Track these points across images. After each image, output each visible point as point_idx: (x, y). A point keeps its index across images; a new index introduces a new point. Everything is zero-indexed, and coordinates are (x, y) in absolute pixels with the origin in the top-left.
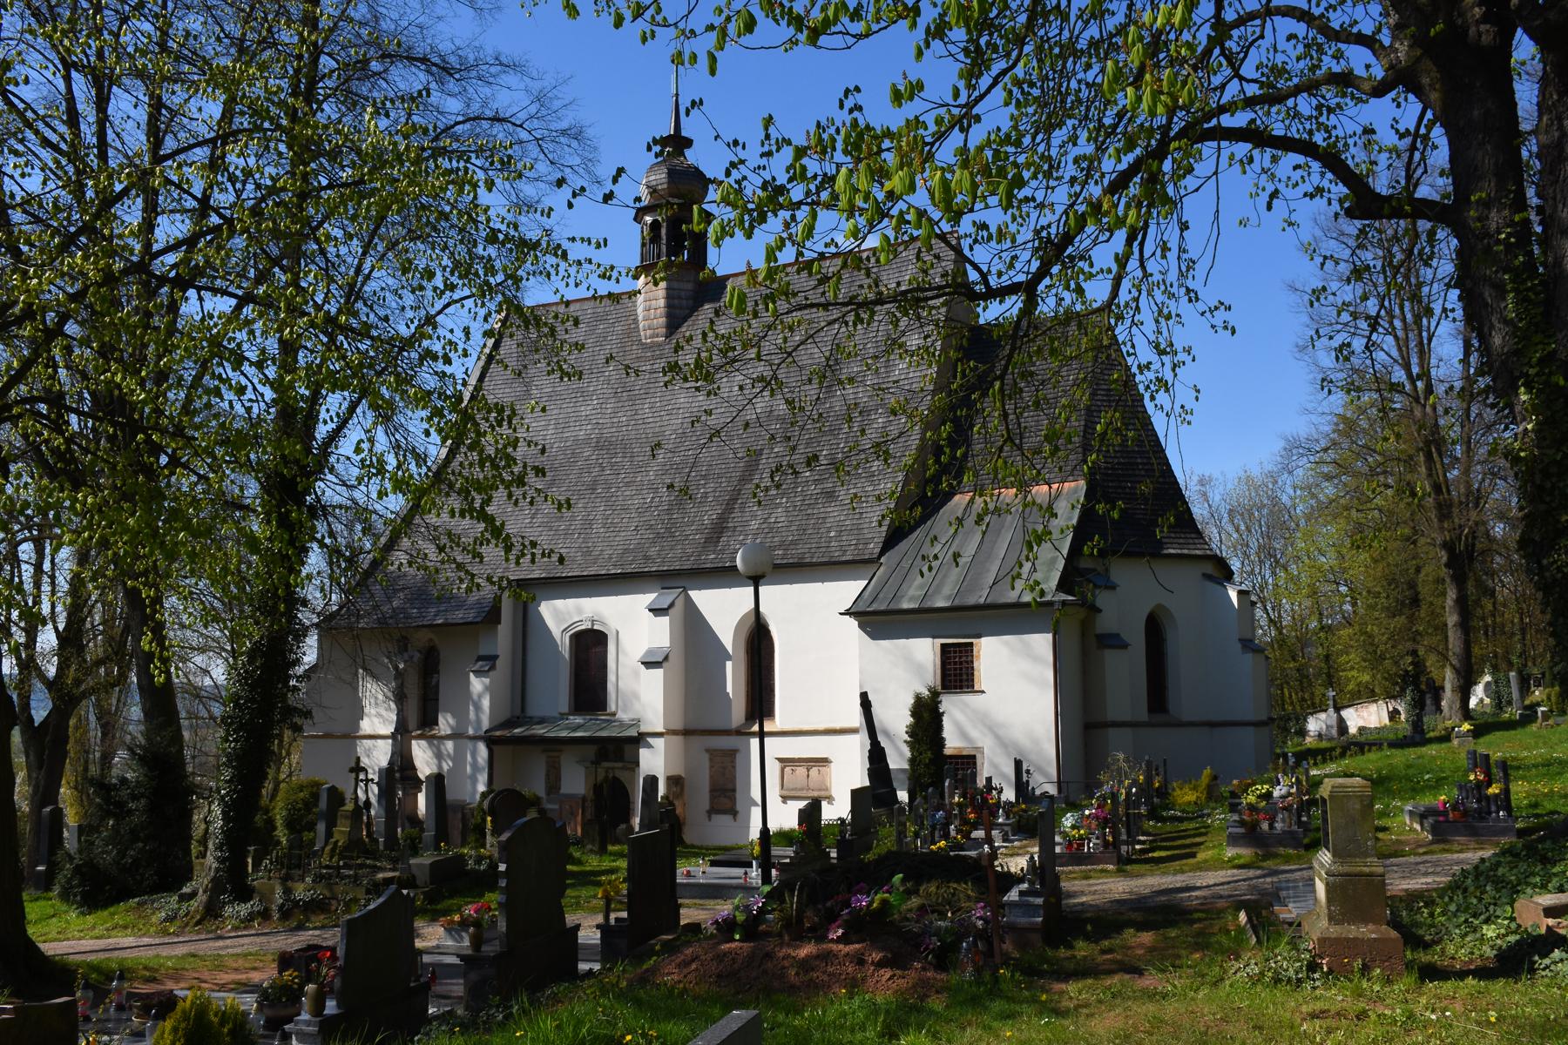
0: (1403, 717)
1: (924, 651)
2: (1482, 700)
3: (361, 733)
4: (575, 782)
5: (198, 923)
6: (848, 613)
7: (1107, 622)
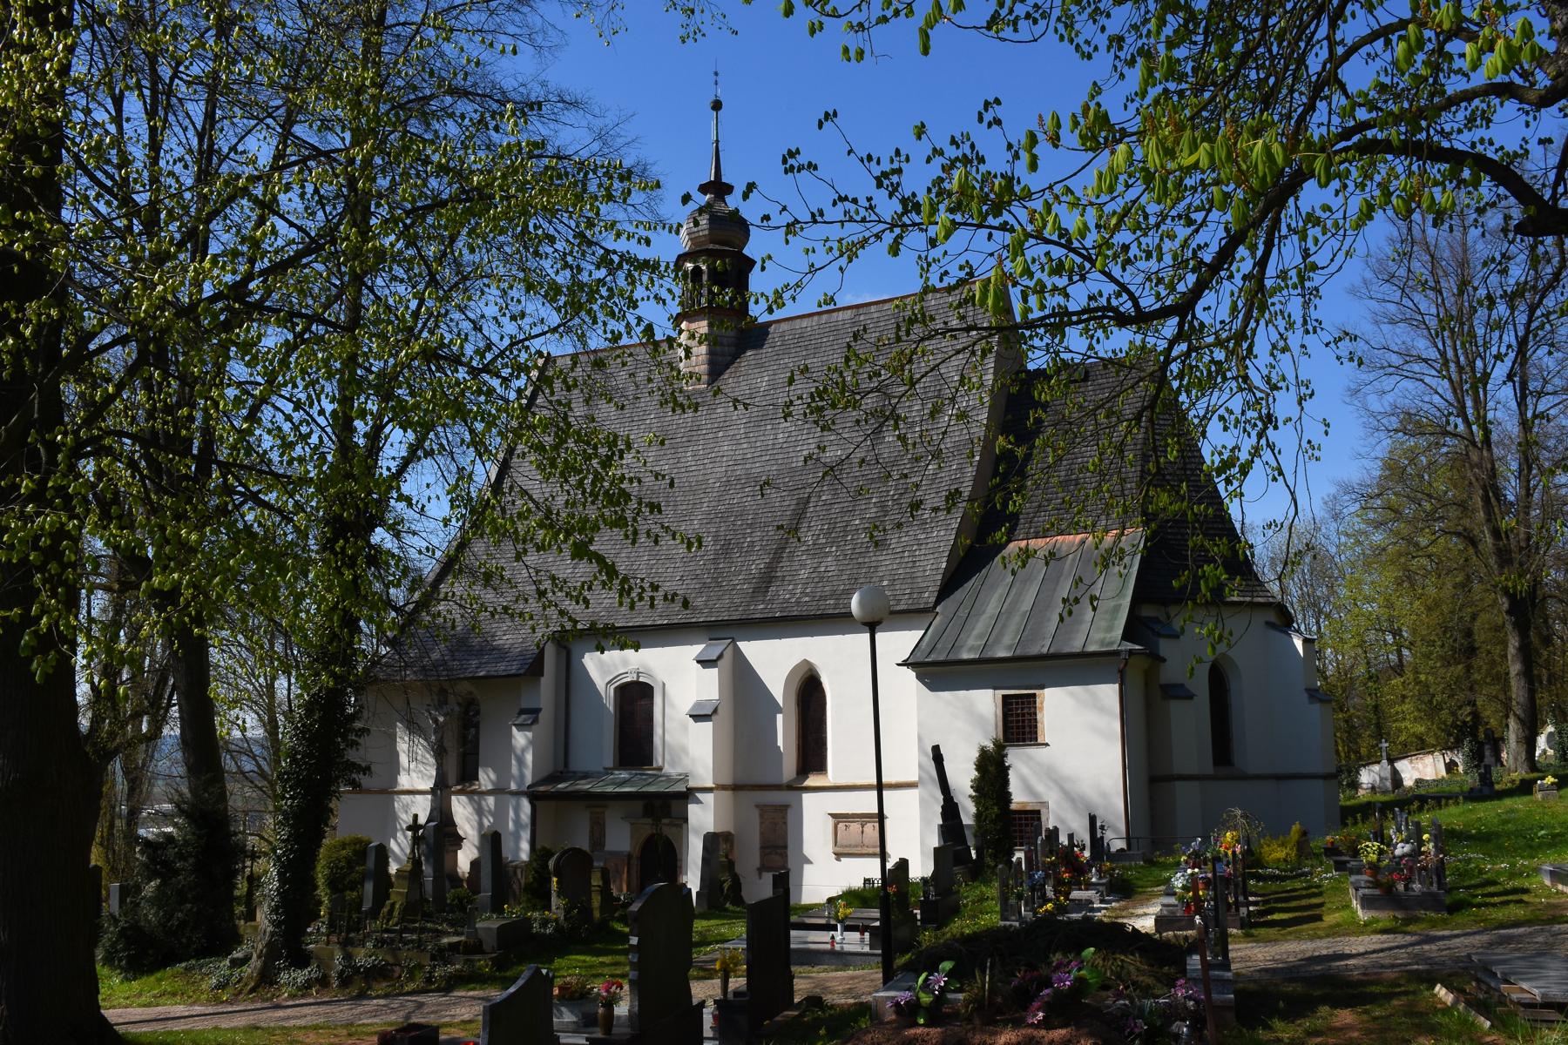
0: (1461, 769)
1: (986, 702)
2: (1544, 752)
3: (399, 788)
4: (621, 838)
5: (253, 990)
6: (905, 664)
7: (1172, 672)
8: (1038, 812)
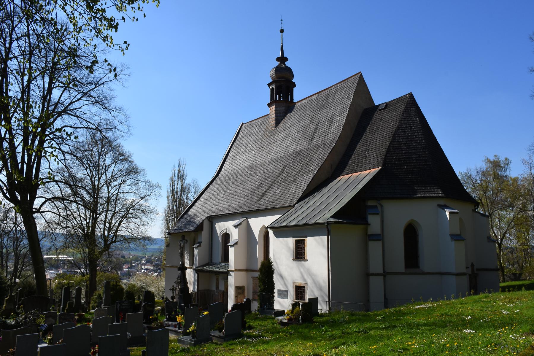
8: (304, 287)
